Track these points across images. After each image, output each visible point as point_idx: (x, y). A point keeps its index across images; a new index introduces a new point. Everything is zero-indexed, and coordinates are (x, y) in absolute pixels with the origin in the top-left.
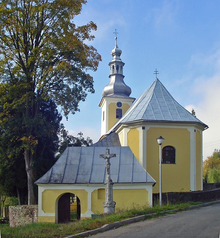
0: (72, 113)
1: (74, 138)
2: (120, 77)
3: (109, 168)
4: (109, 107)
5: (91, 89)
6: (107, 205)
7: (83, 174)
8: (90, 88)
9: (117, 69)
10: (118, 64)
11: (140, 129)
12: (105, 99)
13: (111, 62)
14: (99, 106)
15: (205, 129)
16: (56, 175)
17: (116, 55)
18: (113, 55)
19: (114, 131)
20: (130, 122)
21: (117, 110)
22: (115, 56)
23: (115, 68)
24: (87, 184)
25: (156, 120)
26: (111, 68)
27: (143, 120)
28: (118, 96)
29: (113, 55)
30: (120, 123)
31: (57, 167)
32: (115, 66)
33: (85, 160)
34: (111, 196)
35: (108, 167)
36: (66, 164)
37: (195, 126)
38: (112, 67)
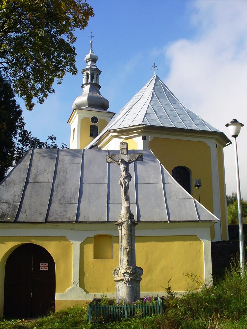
0: (39, 101)
1: (41, 143)
2: (95, 87)
3: (128, 185)
4: (82, 122)
5: (72, 67)
6: (125, 276)
7: (61, 202)
8: (70, 67)
9: (92, 78)
10: (93, 71)
11: (126, 147)
12: (76, 112)
13: (85, 69)
14: (68, 122)
15: (227, 144)
16: (5, 204)
17: (91, 61)
18: (88, 60)
19: (96, 145)
20: (125, 129)
21: (92, 127)
22: (90, 62)
23: (89, 76)
24: (70, 225)
25: (162, 126)
26: (85, 76)
27: (144, 126)
28: (93, 109)
29: (88, 60)
30: (108, 130)
31: (7, 187)
32: (89, 73)
33: (65, 173)
34: (131, 255)
35: (127, 184)
36: (27, 182)
37: (217, 140)
38: (85, 74)
